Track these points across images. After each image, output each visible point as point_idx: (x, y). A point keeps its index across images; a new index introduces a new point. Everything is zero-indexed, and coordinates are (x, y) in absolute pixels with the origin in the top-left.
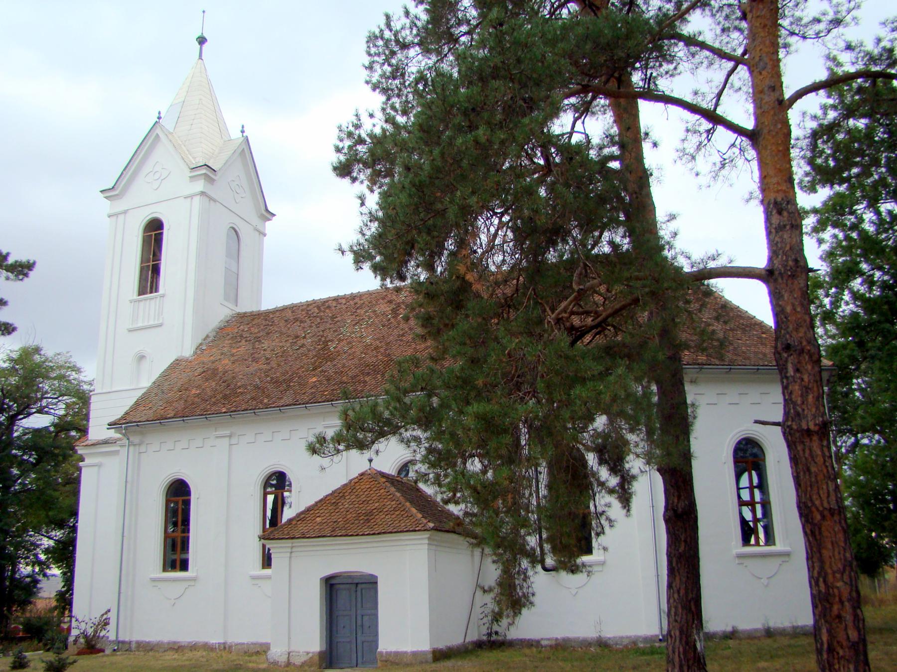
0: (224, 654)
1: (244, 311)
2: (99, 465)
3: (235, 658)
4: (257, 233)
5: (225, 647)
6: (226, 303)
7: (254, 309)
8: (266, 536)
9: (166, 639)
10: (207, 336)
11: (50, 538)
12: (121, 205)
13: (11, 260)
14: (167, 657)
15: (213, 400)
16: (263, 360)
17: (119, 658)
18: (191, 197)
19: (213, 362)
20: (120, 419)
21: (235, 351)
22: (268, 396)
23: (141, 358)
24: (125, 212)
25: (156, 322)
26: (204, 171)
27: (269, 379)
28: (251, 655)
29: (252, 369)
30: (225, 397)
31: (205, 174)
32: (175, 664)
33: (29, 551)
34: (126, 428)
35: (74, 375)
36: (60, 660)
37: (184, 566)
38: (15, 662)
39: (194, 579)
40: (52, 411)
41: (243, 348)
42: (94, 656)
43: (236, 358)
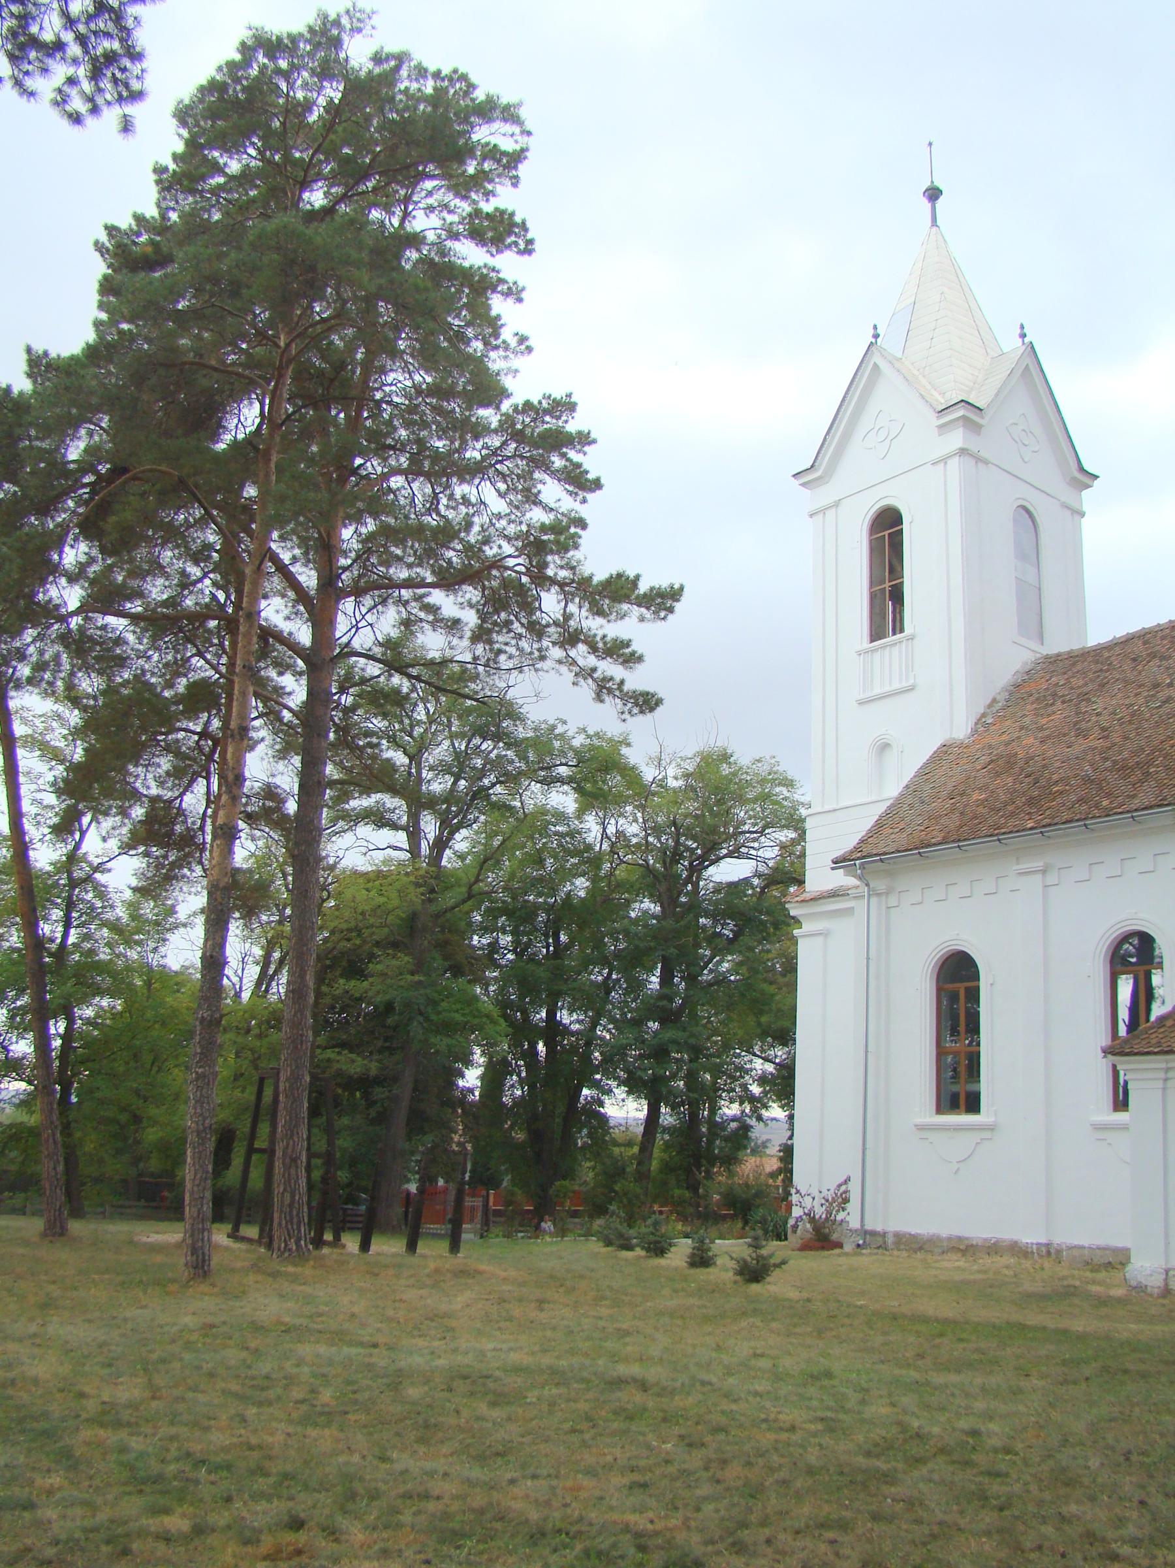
0: (1046, 1265)
1: (1056, 652)
2: (825, 934)
3: (1065, 1273)
4: (1068, 513)
5: (1049, 1252)
6: (1024, 641)
7: (1076, 646)
8: (1116, 1049)
9: (944, 1232)
10: (994, 701)
11: (766, 1059)
12: (826, 494)
13: (643, 587)
14: (946, 1264)
15: (1010, 808)
16: (1096, 732)
17: (865, 1260)
18: (944, 460)
19: (1007, 744)
20: (852, 852)
21: (1044, 721)
22: (1108, 795)
23: (884, 747)
24: (837, 504)
25: (904, 684)
26: (961, 413)
27: (1108, 764)
28: (1096, 1269)
29: (1076, 750)
30: (1031, 801)
31: (963, 417)
32: (958, 1277)
33: (734, 1079)
34: (862, 866)
35: (782, 791)
36: (759, 1258)
37: (973, 1104)
38: (693, 1255)
39: (991, 1128)
40: (753, 852)
41: (1060, 714)
42: (826, 1253)
43: (1047, 733)
